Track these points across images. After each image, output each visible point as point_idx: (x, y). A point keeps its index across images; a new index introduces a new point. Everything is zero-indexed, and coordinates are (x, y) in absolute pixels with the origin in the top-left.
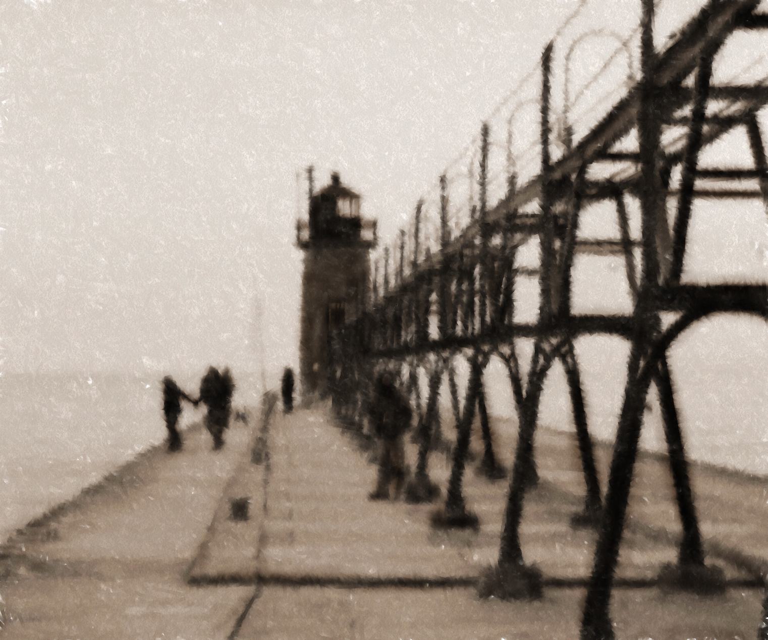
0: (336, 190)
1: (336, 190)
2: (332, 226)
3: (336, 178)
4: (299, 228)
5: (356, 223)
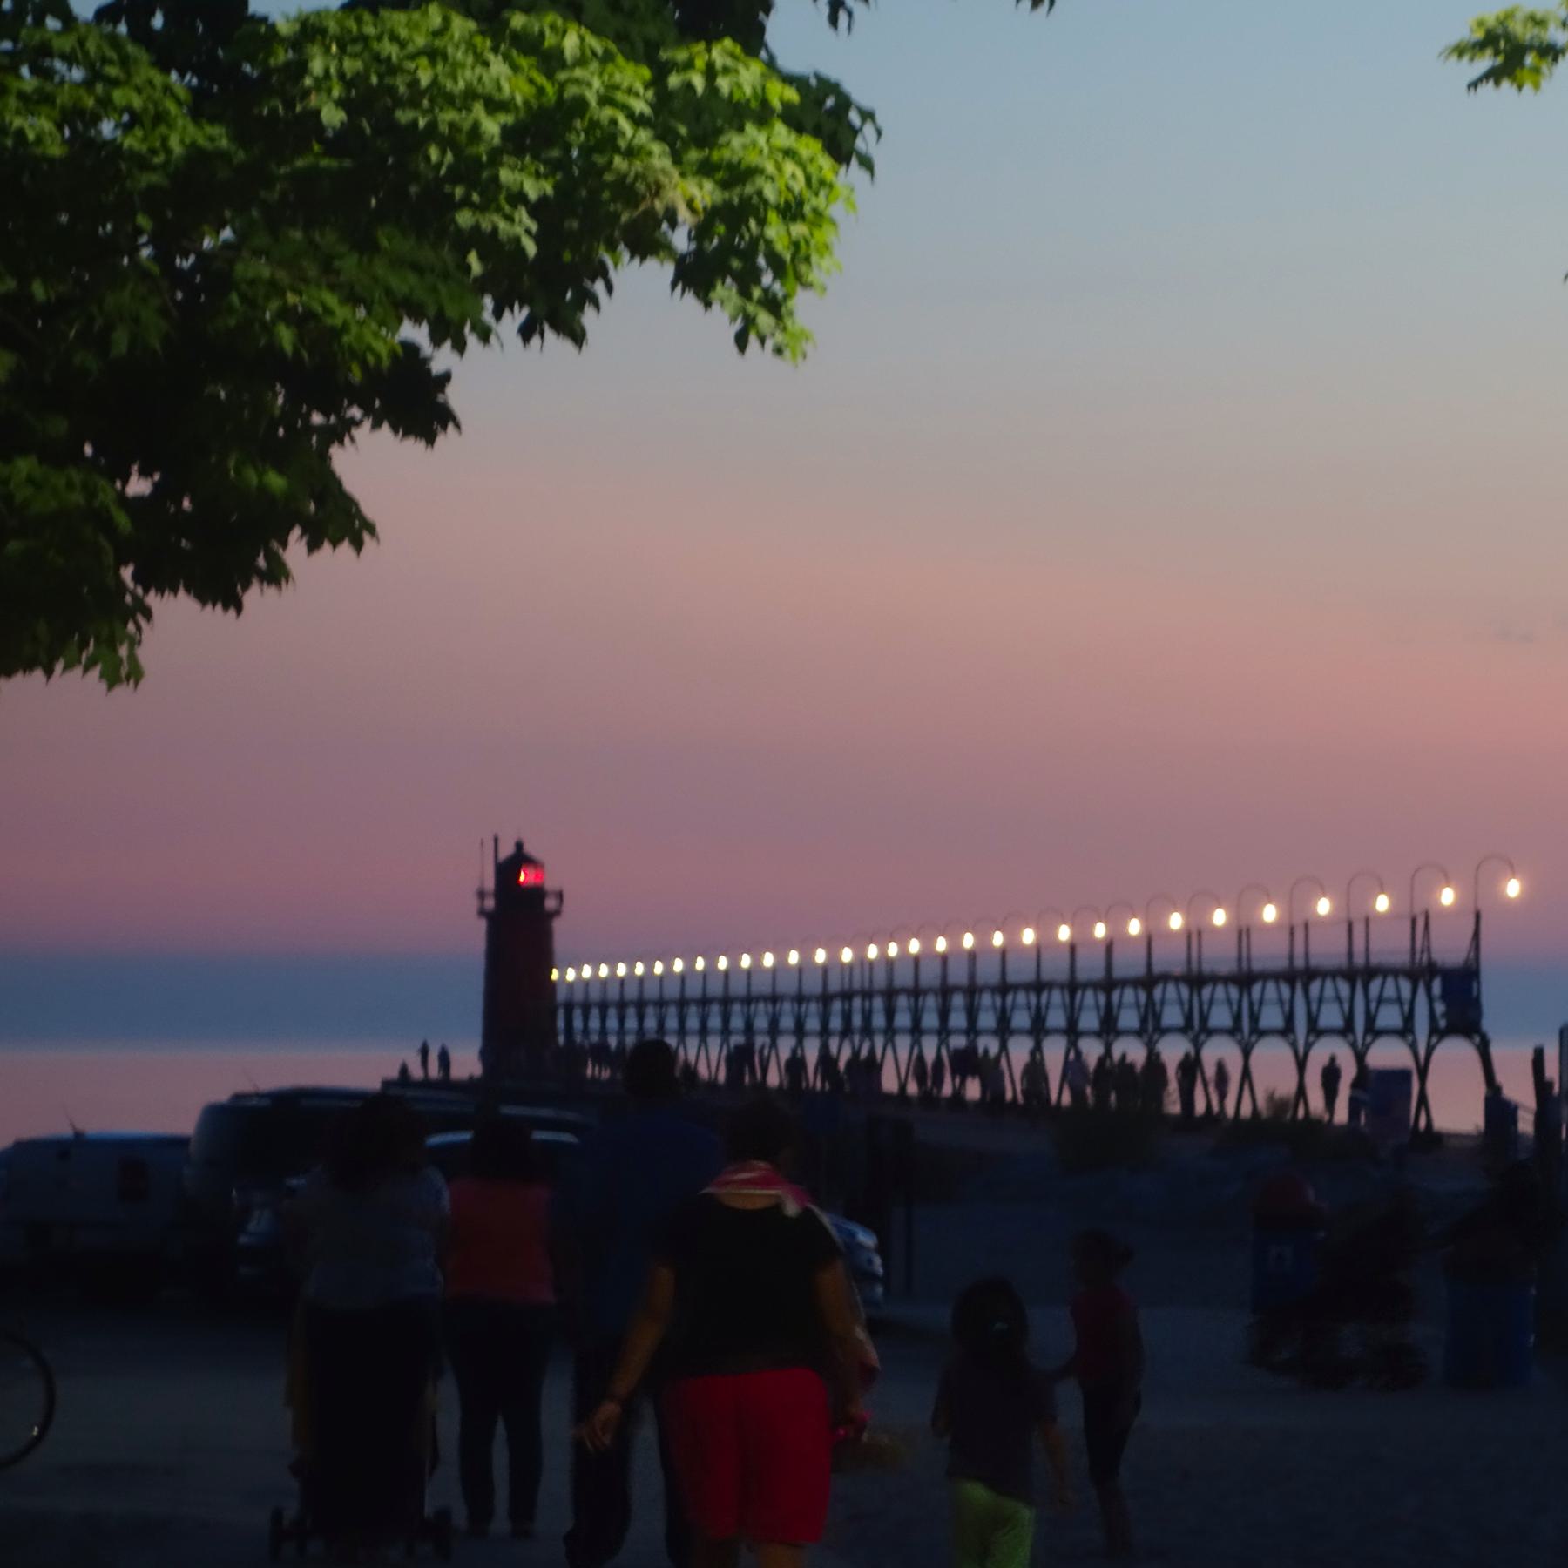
0: (520, 859)
1: (520, 859)
2: (519, 917)
3: (519, 846)
4: (481, 895)
5: (538, 893)
